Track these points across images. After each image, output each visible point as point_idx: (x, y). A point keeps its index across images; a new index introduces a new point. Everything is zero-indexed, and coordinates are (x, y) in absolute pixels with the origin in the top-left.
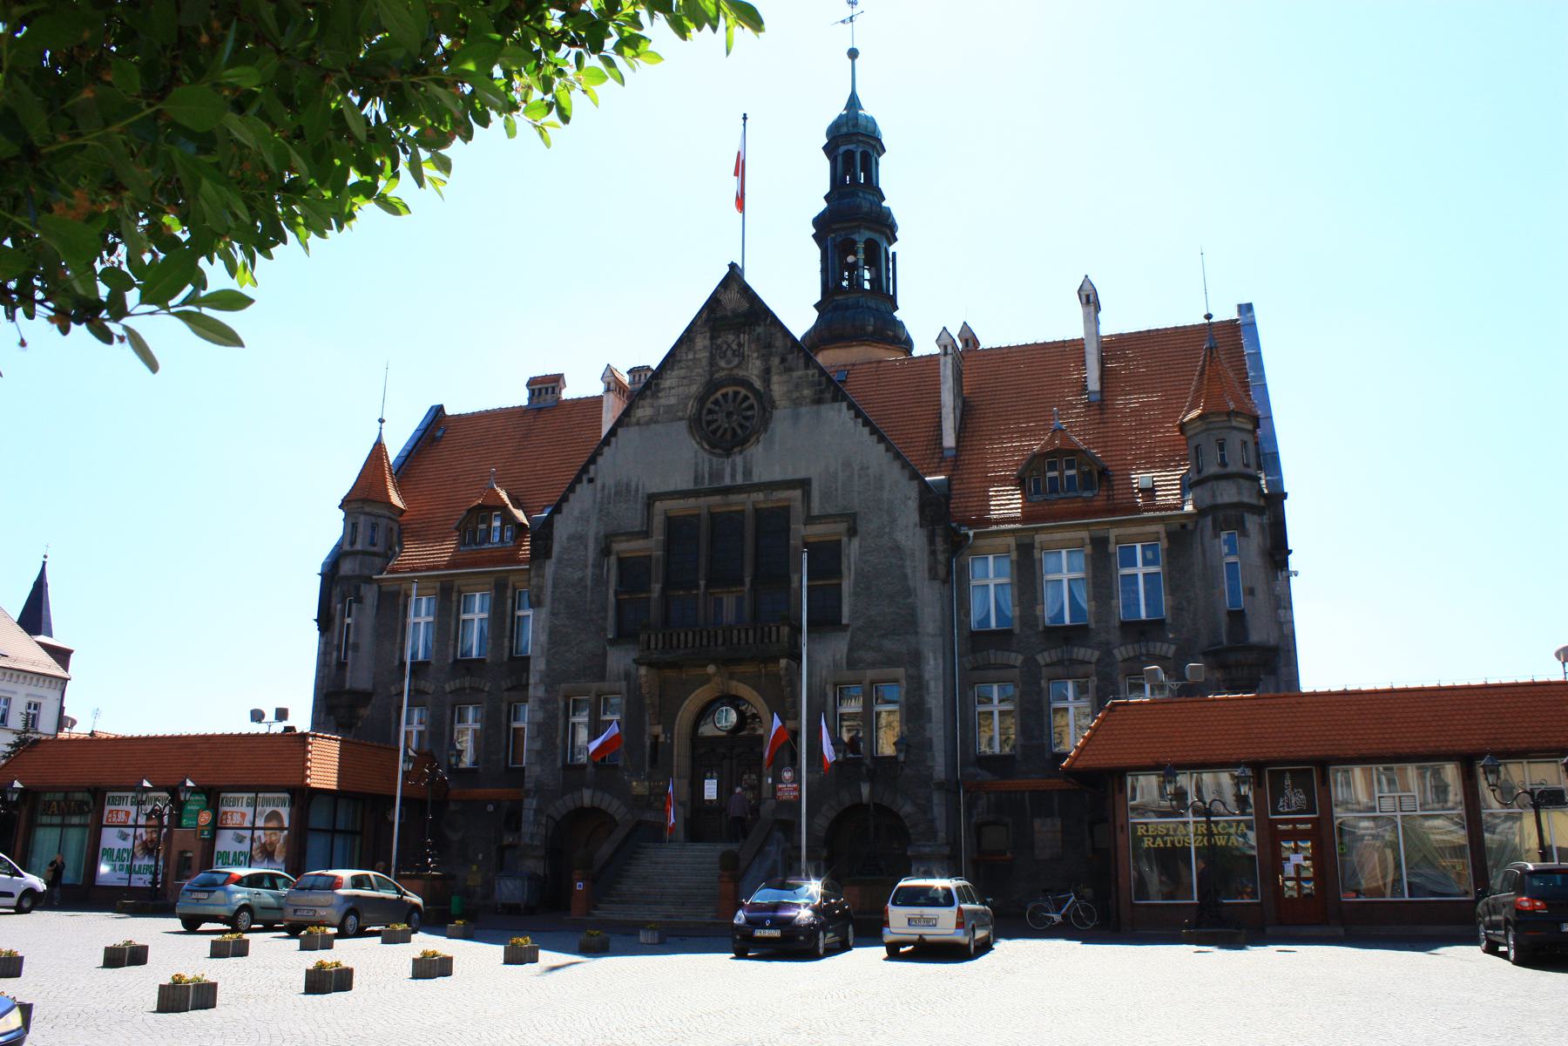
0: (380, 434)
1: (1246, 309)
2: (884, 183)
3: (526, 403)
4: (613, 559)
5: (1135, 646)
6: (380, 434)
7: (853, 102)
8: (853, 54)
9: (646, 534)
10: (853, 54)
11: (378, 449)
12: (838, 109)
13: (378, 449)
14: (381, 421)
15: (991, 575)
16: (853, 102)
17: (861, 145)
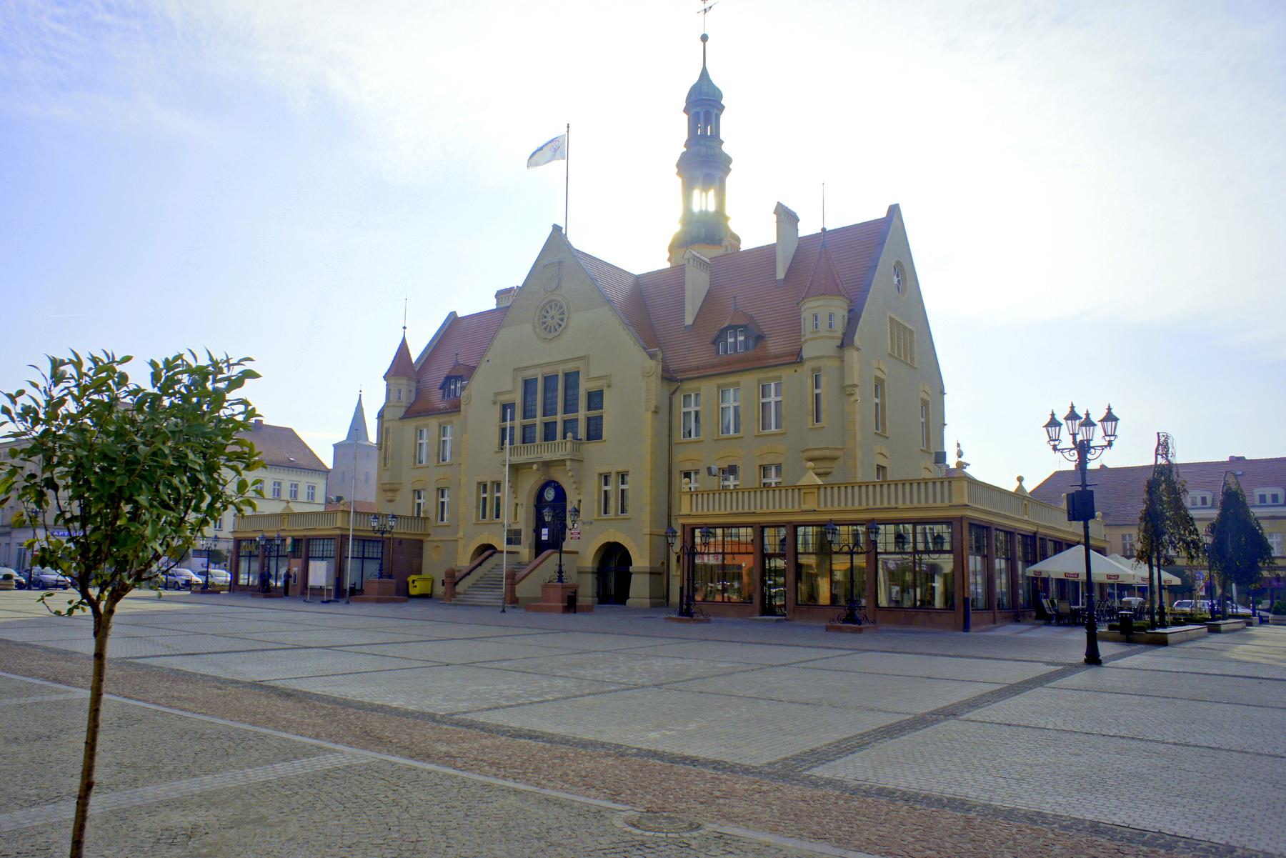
0: (404, 338)
1: (894, 210)
2: (723, 135)
3: (495, 307)
5: (1050, 429)
6: (404, 338)
7: (704, 74)
8: (704, 38)
10: (704, 38)
11: (403, 349)
12: (695, 78)
13: (403, 349)
14: (405, 328)
15: (773, 404)
16: (704, 74)
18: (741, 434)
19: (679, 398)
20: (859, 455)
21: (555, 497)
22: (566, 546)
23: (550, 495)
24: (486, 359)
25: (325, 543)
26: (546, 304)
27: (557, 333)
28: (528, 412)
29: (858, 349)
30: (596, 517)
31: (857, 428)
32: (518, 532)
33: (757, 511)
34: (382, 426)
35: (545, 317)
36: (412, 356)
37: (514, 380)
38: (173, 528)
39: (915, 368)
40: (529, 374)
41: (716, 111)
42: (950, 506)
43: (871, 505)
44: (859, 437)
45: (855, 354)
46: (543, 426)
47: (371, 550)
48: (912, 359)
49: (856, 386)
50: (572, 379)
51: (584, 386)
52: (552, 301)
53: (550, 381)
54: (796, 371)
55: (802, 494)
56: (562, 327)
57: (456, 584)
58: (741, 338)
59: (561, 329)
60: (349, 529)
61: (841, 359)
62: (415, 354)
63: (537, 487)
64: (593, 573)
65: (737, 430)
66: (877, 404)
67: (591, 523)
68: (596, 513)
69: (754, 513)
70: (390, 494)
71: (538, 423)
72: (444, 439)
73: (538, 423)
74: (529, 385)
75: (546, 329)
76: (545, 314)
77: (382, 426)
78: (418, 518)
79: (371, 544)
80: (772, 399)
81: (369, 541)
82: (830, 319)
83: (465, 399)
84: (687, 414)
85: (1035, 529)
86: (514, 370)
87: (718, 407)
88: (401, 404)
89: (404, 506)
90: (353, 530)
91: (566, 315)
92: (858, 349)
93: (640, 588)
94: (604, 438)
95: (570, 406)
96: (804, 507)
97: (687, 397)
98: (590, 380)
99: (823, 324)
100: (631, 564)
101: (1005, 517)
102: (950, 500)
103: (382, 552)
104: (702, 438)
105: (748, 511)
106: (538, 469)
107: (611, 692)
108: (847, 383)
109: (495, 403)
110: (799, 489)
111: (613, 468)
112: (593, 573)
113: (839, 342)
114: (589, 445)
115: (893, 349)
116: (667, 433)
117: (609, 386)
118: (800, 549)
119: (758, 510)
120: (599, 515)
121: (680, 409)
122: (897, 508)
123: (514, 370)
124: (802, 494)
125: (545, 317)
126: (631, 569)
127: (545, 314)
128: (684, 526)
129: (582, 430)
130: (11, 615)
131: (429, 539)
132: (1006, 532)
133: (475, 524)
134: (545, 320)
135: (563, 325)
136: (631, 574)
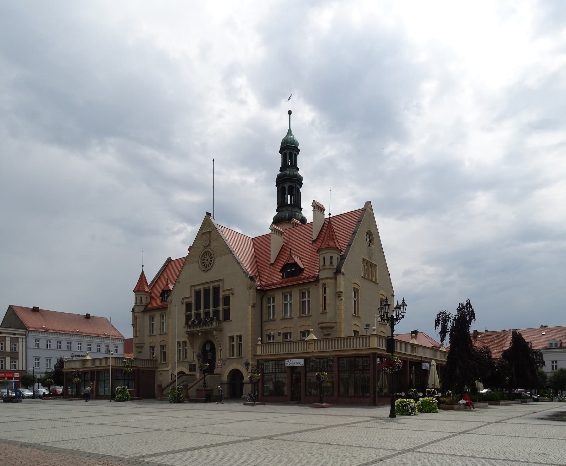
0: (143, 272)
4: (184, 304)
6: (143, 272)
8: (290, 113)
10: (290, 113)
11: (143, 276)
13: (143, 276)
14: (143, 266)
17: (289, 150)
18: (311, 314)
20: (343, 325)
21: (211, 348)
22: (216, 371)
23: (208, 348)
25: (105, 373)
26: (204, 253)
27: (209, 268)
28: (198, 307)
29: (343, 274)
30: (228, 357)
31: (342, 312)
32: (195, 365)
33: (348, 349)
34: (134, 315)
35: (204, 260)
36: (147, 280)
37: (191, 291)
38: (492, 362)
39: (378, 284)
41: (295, 152)
42: (369, 349)
43: (337, 349)
44: (343, 316)
45: (341, 276)
48: (376, 279)
49: (342, 292)
50: (216, 290)
51: (222, 294)
52: (208, 251)
53: (207, 291)
54: (316, 285)
55: (308, 344)
56: (212, 265)
57: (163, 390)
59: (211, 265)
61: (335, 278)
62: (150, 279)
65: (309, 312)
67: (226, 360)
68: (228, 355)
69: (288, 353)
71: (202, 312)
72: (152, 323)
73: (202, 312)
74: (198, 293)
75: (204, 266)
77: (134, 315)
78: (153, 360)
80: (288, 302)
82: (331, 259)
83: (169, 301)
84: (269, 307)
87: (283, 304)
89: (146, 355)
90: (112, 366)
91: (213, 259)
92: (343, 274)
93: (247, 389)
94: (231, 319)
95: (216, 304)
96: (309, 350)
97: (269, 299)
98: (224, 291)
99: (328, 262)
100: (243, 379)
102: (369, 346)
104: (311, 314)
105: (285, 353)
106: (201, 335)
107: (16, 408)
108: (338, 290)
109: (183, 303)
110: (307, 342)
111: (235, 334)
112: (227, 384)
113: (335, 271)
114: (225, 323)
115: (364, 274)
119: (349, 348)
120: (230, 356)
121: (266, 304)
122: (347, 350)
124: (308, 344)
125: (204, 260)
126: (243, 382)
129: (221, 317)
131: (158, 370)
135: (212, 263)
136: (243, 384)
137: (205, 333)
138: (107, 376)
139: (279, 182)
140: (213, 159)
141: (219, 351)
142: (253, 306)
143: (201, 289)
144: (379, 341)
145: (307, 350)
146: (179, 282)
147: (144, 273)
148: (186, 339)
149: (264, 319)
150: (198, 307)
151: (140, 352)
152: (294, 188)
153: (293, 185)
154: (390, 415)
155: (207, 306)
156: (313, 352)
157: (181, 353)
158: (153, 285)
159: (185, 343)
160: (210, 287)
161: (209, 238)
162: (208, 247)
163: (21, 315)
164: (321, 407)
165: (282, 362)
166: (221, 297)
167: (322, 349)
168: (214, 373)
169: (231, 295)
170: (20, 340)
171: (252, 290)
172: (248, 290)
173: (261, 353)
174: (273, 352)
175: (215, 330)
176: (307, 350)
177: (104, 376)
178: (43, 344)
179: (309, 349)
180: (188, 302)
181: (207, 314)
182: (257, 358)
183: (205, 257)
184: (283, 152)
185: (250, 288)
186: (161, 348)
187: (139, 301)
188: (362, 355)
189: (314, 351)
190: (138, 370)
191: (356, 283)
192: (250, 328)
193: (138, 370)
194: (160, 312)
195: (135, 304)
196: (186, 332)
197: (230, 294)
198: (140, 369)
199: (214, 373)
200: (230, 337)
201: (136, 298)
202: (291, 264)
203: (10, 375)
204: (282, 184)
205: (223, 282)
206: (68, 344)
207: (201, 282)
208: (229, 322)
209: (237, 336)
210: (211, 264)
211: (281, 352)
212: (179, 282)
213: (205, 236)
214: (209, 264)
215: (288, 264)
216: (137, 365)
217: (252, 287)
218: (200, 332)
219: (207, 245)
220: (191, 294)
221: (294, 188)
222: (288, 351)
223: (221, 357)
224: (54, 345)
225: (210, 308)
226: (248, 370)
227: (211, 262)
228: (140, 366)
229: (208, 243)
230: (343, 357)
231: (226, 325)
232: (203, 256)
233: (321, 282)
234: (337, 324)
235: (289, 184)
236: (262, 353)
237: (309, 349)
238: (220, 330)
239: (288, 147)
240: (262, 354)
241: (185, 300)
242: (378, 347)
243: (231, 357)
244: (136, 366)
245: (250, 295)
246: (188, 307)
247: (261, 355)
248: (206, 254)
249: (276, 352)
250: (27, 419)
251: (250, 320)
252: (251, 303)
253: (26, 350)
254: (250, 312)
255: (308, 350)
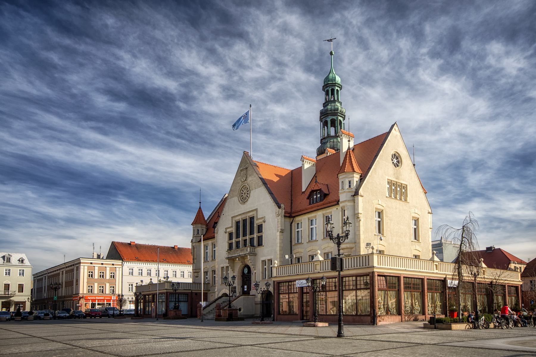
0: (200, 208)
4: (227, 233)
6: (200, 208)
9: (232, 227)
14: (200, 203)
17: (330, 87)
19: (294, 225)
23: (246, 271)
24: (223, 214)
28: (238, 236)
40: (237, 219)
42: (348, 269)
46: (243, 241)
47: (182, 297)
50: (252, 219)
51: (256, 222)
53: (245, 221)
54: (337, 209)
56: (248, 197)
58: (319, 196)
60: (201, 290)
61: (354, 201)
63: (241, 268)
64: (260, 304)
66: (344, 216)
69: (298, 275)
70: (196, 274)
73: (241, 240)
76: (242, 192)
79: (182, 295)
81: (181, 294)
84: (298, 232)
85: (490, 280)
86: (232, 217)
88: (199, 235)
94: (263, 245)
101: (514, 281)
102: (369, 265)
103: (188, 299)
112: (260, 304)
113: (353, 194)
116: (408, 257)
117: (264, 222)
118: (344, 289)
123: (232, 217)
127: (242, 192)
128: (274, 282)
130: (236, 329)
131: (210, 292)
132: (515, 287)
133: (221, 285)
134: (242, 194)
137: (243, 257)
138: (382, 281)
139: (322, 117)
140: (250, 105)
141: (254, 274)
142: (282, 231)
143: (240, 219)
144: (379, 259)
145: (314, 271)
146: (223, 214)
147: (201, 209)
148: (228, 265)
149: (293, 243)
150: (238, 236)
151: (197, 277)
152: (336, 120)
153: (335, 117)
154: (337, 335)
155: (244, 235)
156: (319, 272)
157: (267, 272)
158: (211, 218)
159: (227, 267)
160: (247, 217)
161: (246, 174)
162: (245, 182)
163: (121, 249)
164: (313, 325)
165: (289, 284)
166: (255, 225)
167: (302, 272)
168: (250, 294)
169: (263, 223)
170: (117, 269)
171: (280, 217)
172: (277, 217)
173: (277, 275)
174: (286, 274)
175: (249, 255)
176: (314, 271)
177: (292, 288)
178: (136, 272)
179: (316, 269)
180: (230, 231)
181: (238, 243)
182: (273, 280)
183: (243, 191)
184: (326, 90)
185: (278, 215)
186: (212, 273)
187: (196, 233)
188: (362, 274)
189: (320, 272)
190: (192, 293)
191: (379, 204)
192: (278, 252)
193: (192, 293)
194: (212, 241)
195: (193, 235)
196: (227, 258)
197: (262, 222)
198: (193, 291)
199: (250, 294)
200: (263, 261)
201: (194, 230)
202: (316, 191)
203: (109, 298)
204: (324, 119)
205: (257, 212)
206: (139, 270)
207: (240, 213)
208: (262, 248)
209: (269, 260)
210: (247, 196)
211: (292, 273)
212: (223, 214)
213: (243, 172)
214: (246, 197)
215: (313, 191)
216: (190, 288)
217: (279, 215)
218: (237, 257)
219: (244, 180)
220: (232, 224)
221: (336, 120)
222: (299, 273)
223: (255, 280)
224: (136, 272)
225: (247, 236)
226: (257, 291)
227: (247, 195)
228: (193, 289)
229: (245, 179)
230: (283, 282)
231: (259, 250)
232: (242, 190)
233: (341, 205)
234: (356, 244)
235: (331, 117)
236: (278, 274)
237: (316, 269)
238: (255, 254)
239: (330, 85)
240: (277, 276)
241: (228, 230)
242: (379, 266)
243: (264, 279)
244: (189, 289)
245: (278, 222)
246: (231, 235)
247: (276, 277)
248: (244, 188)
249: (288, 274)
250: (134, 332)
251: (279, 245)
252: (280, 228)
253: (122, 277)
254: (278, 237)
255: (315, 270)
